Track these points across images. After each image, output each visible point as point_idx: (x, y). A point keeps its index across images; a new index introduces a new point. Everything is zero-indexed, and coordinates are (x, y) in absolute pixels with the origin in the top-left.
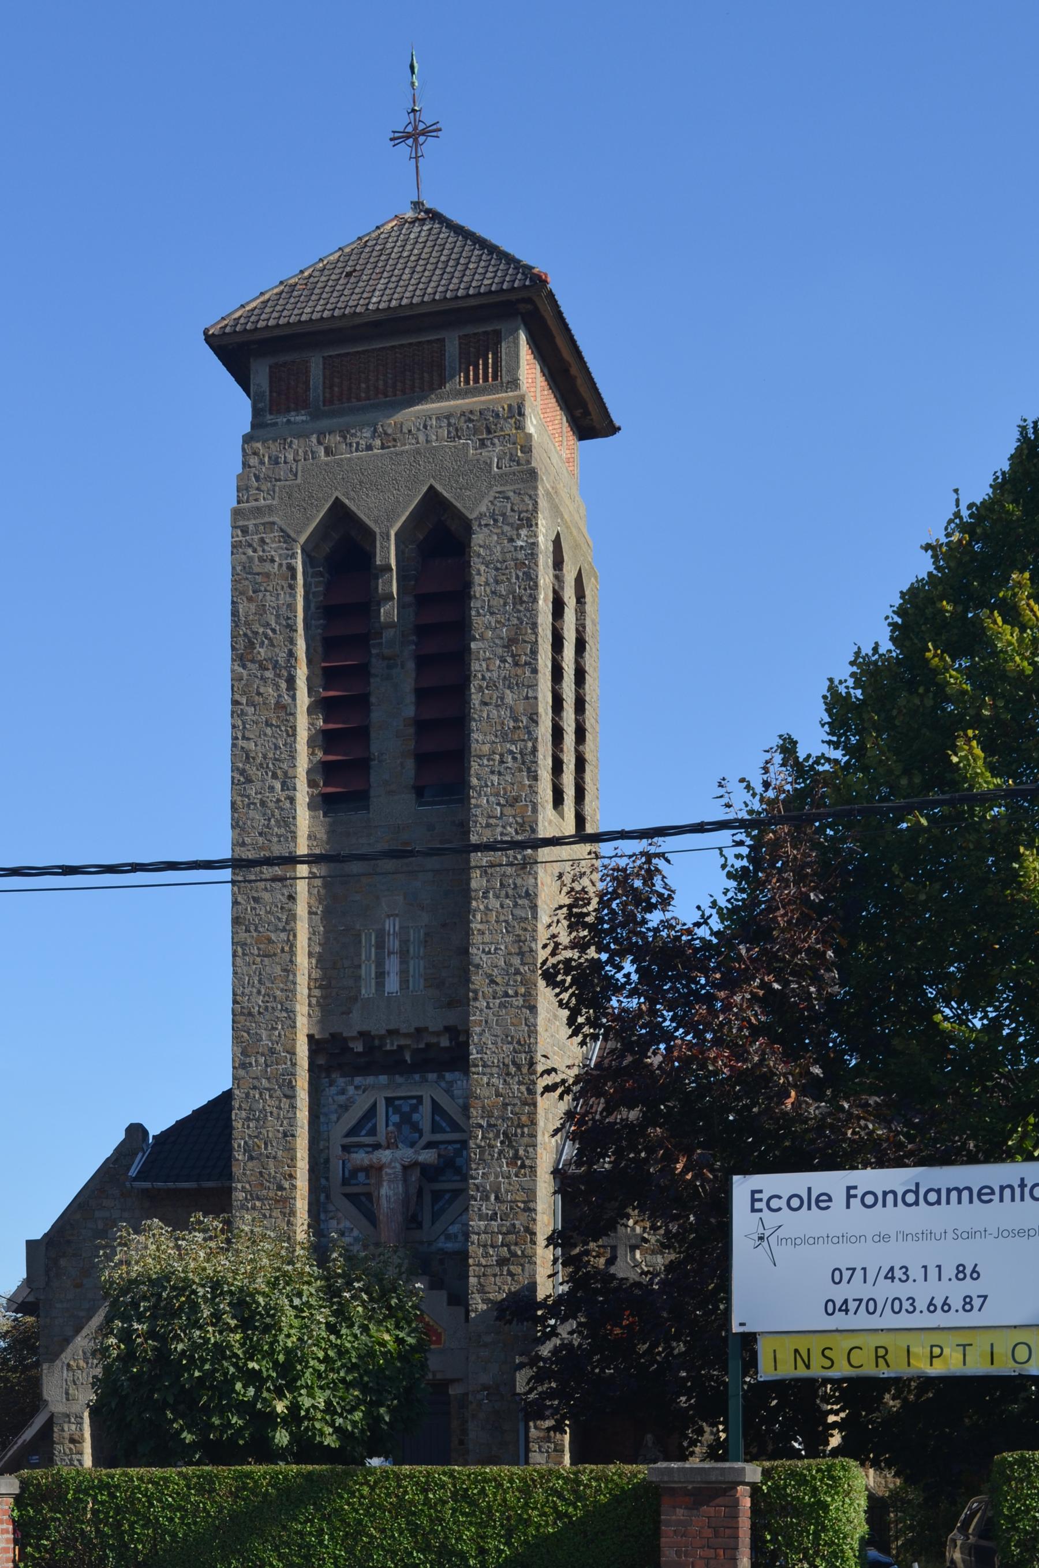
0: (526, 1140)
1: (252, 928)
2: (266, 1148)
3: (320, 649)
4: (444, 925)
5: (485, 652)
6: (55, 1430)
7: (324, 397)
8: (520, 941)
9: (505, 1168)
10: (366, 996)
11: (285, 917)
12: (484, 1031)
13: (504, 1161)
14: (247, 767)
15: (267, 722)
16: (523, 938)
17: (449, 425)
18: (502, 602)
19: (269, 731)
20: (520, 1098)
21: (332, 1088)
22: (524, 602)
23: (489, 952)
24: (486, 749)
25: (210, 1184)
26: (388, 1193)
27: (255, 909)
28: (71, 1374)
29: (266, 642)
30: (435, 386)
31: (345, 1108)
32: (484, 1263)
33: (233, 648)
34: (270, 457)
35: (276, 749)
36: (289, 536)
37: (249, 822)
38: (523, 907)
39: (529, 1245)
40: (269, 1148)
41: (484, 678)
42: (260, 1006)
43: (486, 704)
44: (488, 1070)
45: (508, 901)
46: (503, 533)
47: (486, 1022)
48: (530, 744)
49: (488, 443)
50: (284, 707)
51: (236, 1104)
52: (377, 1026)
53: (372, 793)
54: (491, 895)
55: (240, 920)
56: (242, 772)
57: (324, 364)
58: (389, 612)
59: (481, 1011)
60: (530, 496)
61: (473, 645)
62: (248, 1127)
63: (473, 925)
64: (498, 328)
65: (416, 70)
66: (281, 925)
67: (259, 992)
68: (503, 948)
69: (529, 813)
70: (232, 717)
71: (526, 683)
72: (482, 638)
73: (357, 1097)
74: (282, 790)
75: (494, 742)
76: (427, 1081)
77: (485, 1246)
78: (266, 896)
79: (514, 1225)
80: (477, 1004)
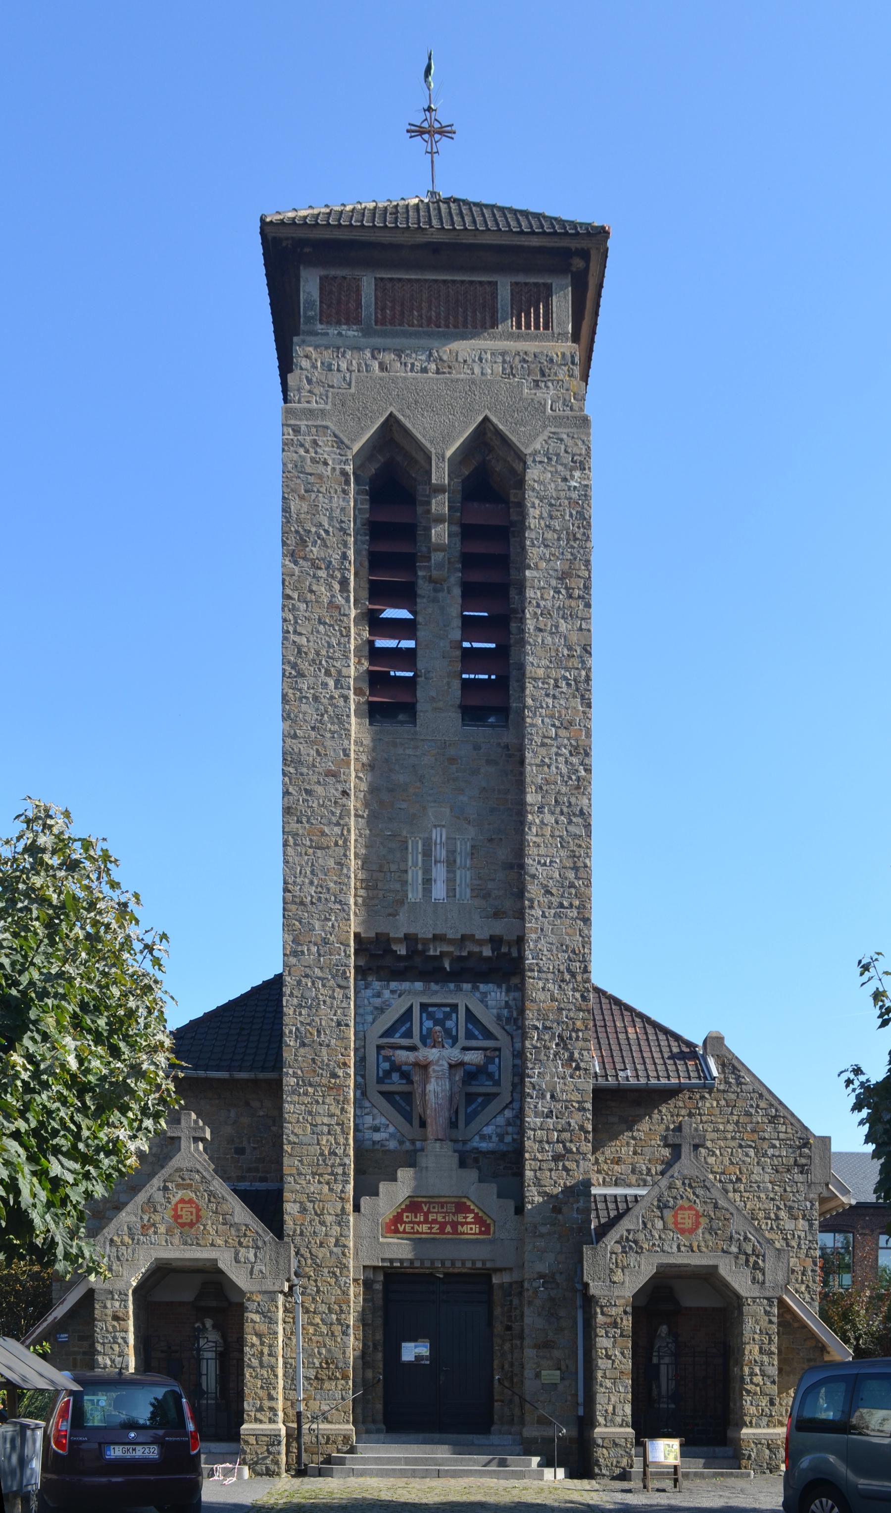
0: (580, 1044)
1: (304, 820)
2: (319, 1036)
3: (366, 564)
4: (490, 840)
5: (539, 581)
6: (97, 1306)
7: (376, 317)
8: (574, 856)
9: (560, 1069)
10: (413, 900)
11: (338, 812)
12: (540, 938)
13: (560, 1062)
14: (299, 661)
15: (319, 619)
16: (577, 854)
17: (504, 362)
18: (556, 536)
19: (321, 628)
20: (574, 1004)
21: (368, 991)
22: (578, 539)
23: (545, 864)
24: (541, 672)
25: (244, 1075)
26: (436, 1090)
27: (307, 801)
28: (114, 1249)
29: (319, 542)
30: (488, 324)
31: (381, 1010)
32: (540, 1158)
33: (284, 544)
34: (322, 363)
35: (329, 647)
36: (342, 443)
37: (301, 716)
38: (577, 825)
39: (584, 1143)
40: (322, 1036)
41: (538, 606)
42: (312, 897)
43: (540, 630)
44: (543, 975)
45: (562, 818)
46: (556, 472)
47: (542, 930)
48: (583, 673)
49: (543, 385)
50: (338, 608)
51: (287, 990)
52: (424, 931)
53: (419, 707)
54: (546, 810)
55: (292, 811)
56: (294, 666)
57: (376, 285)
58: (440, 533)
59: (537, 919)
60: (583, 441)
61: (528, 573)
62: (300, 1014)
63: (529, 838)
64: (549, 281)
65: (432, 71)
66: (334, 820)
67: (311, 883)
68: (558, 861)
69: (583, 737)
70: (283, 610)
71: (580, 615)
72: (537, 568)
73: (392, 1001)
74: (336, 688)
75: (548, 667)
76: (461, 990)
77: (541, 1142)
78: (320, 790)
79: (569, 1124)
80: (533, 912)
